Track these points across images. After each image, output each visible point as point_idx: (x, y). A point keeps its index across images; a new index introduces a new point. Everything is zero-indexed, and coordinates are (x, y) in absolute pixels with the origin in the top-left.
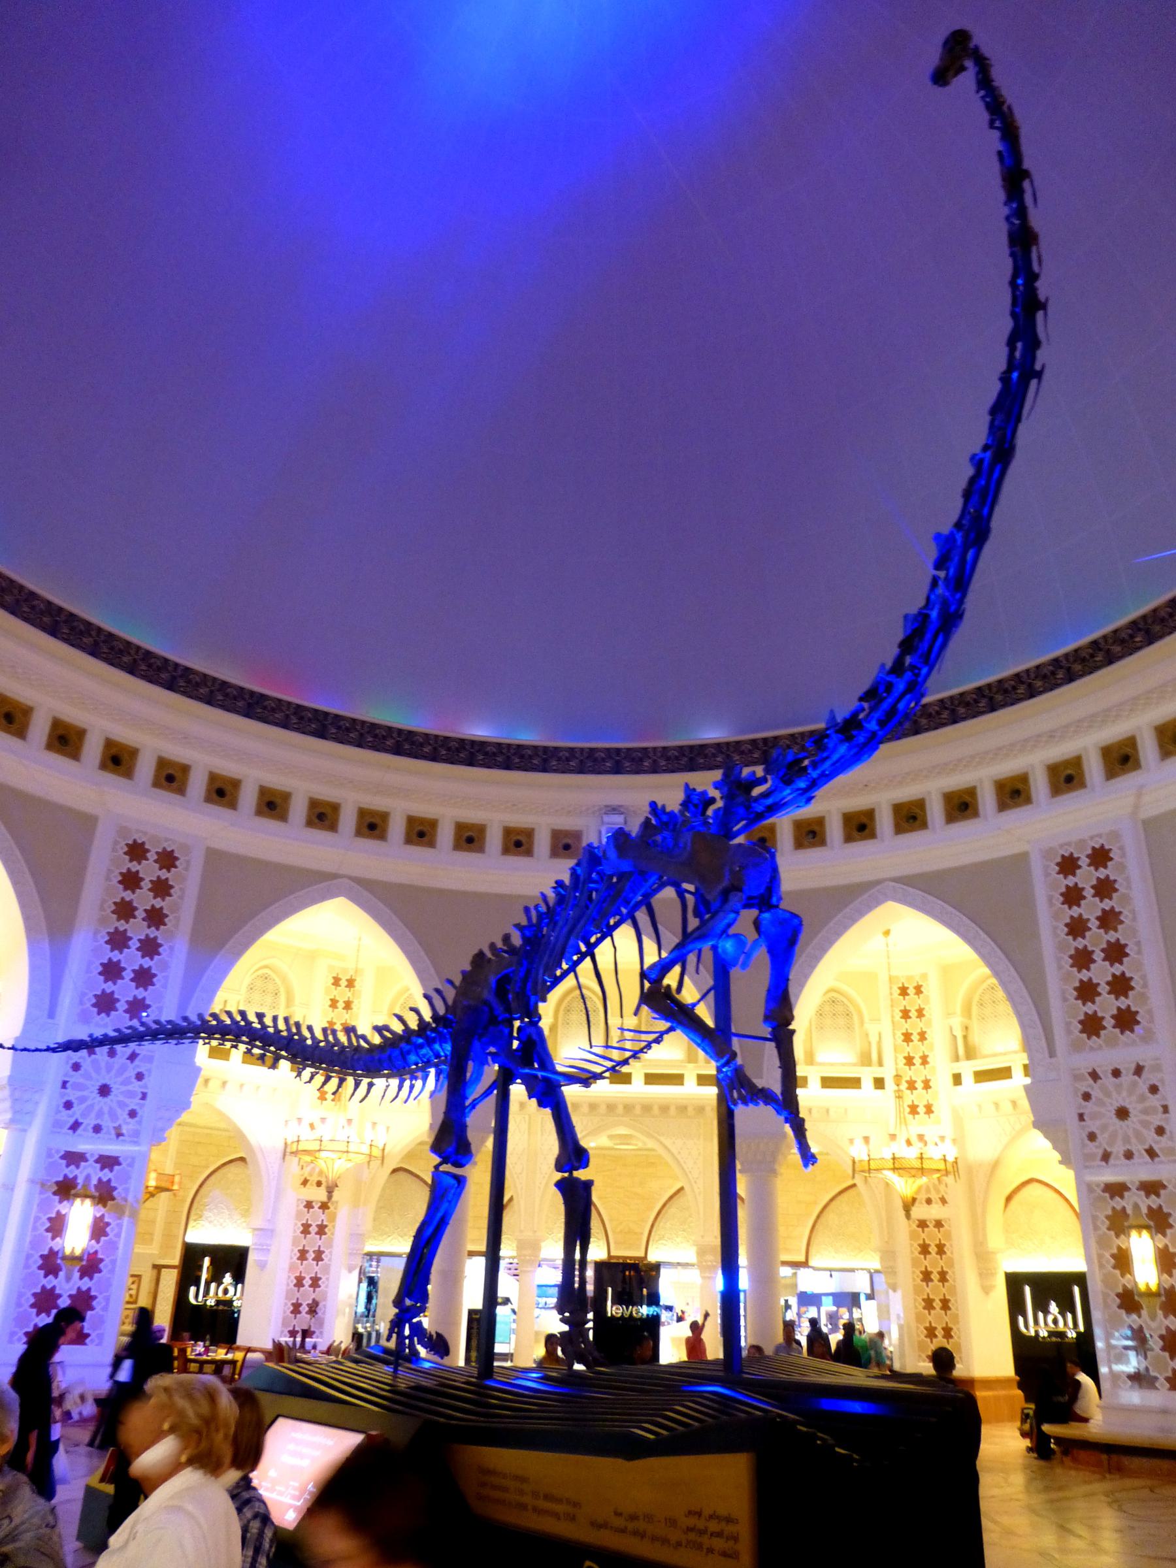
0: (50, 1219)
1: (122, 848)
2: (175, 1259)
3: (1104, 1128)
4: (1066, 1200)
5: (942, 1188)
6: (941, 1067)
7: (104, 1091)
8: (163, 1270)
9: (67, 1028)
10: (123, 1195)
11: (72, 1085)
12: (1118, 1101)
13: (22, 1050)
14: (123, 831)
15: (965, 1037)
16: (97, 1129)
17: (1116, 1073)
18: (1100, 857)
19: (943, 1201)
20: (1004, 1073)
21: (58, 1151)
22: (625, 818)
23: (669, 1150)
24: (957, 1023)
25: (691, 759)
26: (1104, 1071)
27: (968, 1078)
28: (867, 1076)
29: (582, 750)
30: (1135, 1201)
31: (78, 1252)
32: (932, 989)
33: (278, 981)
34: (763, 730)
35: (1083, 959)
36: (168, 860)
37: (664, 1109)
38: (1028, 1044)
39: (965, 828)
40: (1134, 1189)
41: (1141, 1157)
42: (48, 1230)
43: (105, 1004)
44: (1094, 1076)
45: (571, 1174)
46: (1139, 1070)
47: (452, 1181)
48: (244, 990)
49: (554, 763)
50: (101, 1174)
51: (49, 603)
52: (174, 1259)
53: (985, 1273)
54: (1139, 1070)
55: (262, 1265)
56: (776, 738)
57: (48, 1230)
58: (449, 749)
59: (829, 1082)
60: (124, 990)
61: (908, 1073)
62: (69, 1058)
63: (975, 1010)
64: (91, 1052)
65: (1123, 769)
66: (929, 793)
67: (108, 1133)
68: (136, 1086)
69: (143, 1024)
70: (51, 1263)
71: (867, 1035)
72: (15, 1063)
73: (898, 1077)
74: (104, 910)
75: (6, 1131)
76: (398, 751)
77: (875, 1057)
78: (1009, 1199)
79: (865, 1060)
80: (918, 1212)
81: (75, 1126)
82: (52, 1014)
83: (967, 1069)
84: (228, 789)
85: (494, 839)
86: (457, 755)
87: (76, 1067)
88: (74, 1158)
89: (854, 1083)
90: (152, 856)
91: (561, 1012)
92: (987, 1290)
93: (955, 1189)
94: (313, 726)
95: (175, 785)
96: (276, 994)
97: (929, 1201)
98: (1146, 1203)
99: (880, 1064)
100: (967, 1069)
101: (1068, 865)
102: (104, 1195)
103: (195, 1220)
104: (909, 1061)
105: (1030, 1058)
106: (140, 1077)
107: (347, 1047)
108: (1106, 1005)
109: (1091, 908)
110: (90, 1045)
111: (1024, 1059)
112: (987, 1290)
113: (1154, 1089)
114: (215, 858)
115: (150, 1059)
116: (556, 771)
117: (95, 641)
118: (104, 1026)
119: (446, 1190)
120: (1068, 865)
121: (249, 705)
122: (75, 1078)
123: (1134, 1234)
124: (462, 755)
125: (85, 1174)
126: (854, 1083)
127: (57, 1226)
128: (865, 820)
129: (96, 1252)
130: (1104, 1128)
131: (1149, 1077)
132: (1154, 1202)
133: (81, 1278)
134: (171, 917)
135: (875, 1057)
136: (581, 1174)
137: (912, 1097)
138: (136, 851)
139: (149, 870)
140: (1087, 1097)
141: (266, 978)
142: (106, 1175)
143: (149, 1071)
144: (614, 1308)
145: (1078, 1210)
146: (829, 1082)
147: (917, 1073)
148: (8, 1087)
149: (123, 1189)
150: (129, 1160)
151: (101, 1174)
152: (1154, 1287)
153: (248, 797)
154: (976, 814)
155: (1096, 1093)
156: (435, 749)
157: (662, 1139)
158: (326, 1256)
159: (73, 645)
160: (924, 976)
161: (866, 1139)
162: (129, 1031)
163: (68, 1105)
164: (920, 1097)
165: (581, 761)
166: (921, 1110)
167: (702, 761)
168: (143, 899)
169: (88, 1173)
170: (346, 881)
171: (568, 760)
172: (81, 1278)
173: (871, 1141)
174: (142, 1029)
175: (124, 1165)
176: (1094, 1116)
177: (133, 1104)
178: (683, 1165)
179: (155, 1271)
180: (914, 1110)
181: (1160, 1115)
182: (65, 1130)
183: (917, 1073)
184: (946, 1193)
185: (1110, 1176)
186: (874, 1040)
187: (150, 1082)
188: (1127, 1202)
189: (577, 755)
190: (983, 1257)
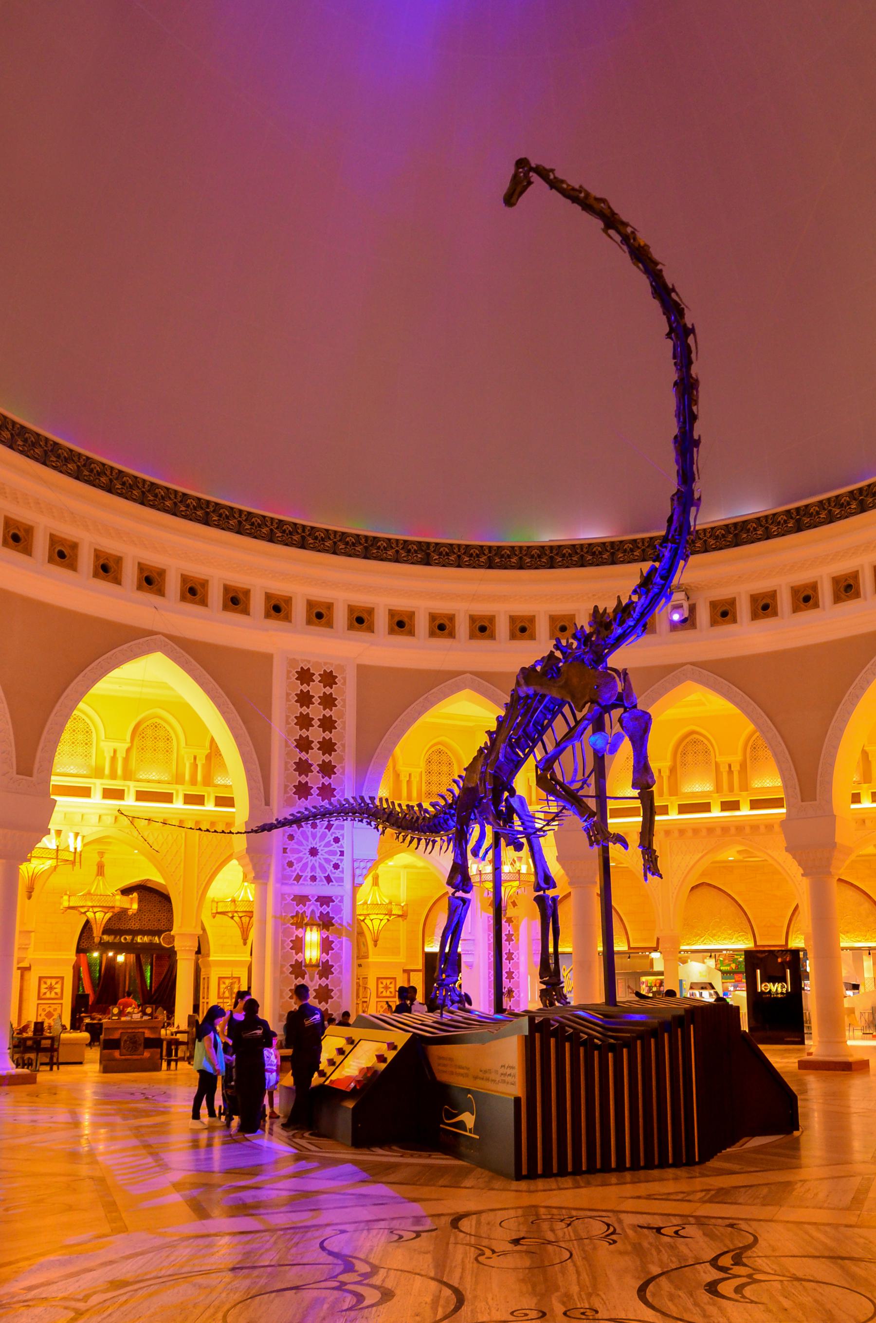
1: (294, 676)
2: (420, 964)
7: (314, 852)
8: (411, 973)
9: (278, 811)
10: (339, 922)
11: (290, 850)
13: (236, 833)
14: (292, 662)
16: (313, 879)
22: (686, 594)
23: (776, 860)
25: (736, 535)
29: (643, 540)
31: (314, 961)
33: (449, 753)
34: (796, 501)
36: (329, 679)
37: (696, 831)
39: (808, 616)
40: (313, 900)
43: (303, 790)
45: (544, 892)
47: (460, 902)
48: (422, 764)
49: (621, 555)
50: (321, 909)
51: (199, 499)
52: (418, 965)
55: (470, 966)
56: (807, 506)
58: (532, 557)
60: (315, 780)
62: (285, 832)
64: (300, 826)
65: (724, 621)
66: (821, 577)
67: (321, 881)
68: (335, 847)
69: (331, 804)
70: (299, 969)
72: (247, 838)
74: (289, 724)
75: (253, 886)
76: (490, 565)
82: (267, 803)
84: (365, 616)
86: (540, 561)
87: (291, 837)
88: (302, 899)
90: (317, 678)
91: (679, 755)
94: (419, 556)
95: (324, 620)
96: (450, 764)
98: (319, 909)
102: (326, 922)
103: (430, 936)
106: (337, 840)
110: (296, 821)
114: (363, 671)
115: (342, 827)
116: (622, 562)
117: (239, 521)
118: (301, 806)
119: (457, 907)
121: (366, 548)
122: (293, 845)
124: (544, 560)
125: (310, 910)
127: (299, 945)
128: (809, 592)
129: (327, 961)
133: (320, 979)
134: (339, 722)
136: (551, 893)
138: (305, 676)
139: (317, 689)
141: (440, 752)
142: (325, 909)
143: (343, 835)
144: (763, 985)
148: (247, 855)
150: (340, 898)
151: (321, 909)
153: (381, 621)
154: (816, 605)
156: (521, 558)
157: (769, 852)
158: (515, 956)
159: (223, 529)
162: (299, 815)
163: (291, 864)
165: (643, 551)
167: (745, 536)
168: (316, 711)
171: (632, 550)
172: (320, 979)
174: (306, 813)
175: (336, 901)
177: (335, 859)
178: (789, 872)
179: (406, 975)
181: (338, 857)
184: (517, 899)
187: (345, 843)
189: (639, 545)
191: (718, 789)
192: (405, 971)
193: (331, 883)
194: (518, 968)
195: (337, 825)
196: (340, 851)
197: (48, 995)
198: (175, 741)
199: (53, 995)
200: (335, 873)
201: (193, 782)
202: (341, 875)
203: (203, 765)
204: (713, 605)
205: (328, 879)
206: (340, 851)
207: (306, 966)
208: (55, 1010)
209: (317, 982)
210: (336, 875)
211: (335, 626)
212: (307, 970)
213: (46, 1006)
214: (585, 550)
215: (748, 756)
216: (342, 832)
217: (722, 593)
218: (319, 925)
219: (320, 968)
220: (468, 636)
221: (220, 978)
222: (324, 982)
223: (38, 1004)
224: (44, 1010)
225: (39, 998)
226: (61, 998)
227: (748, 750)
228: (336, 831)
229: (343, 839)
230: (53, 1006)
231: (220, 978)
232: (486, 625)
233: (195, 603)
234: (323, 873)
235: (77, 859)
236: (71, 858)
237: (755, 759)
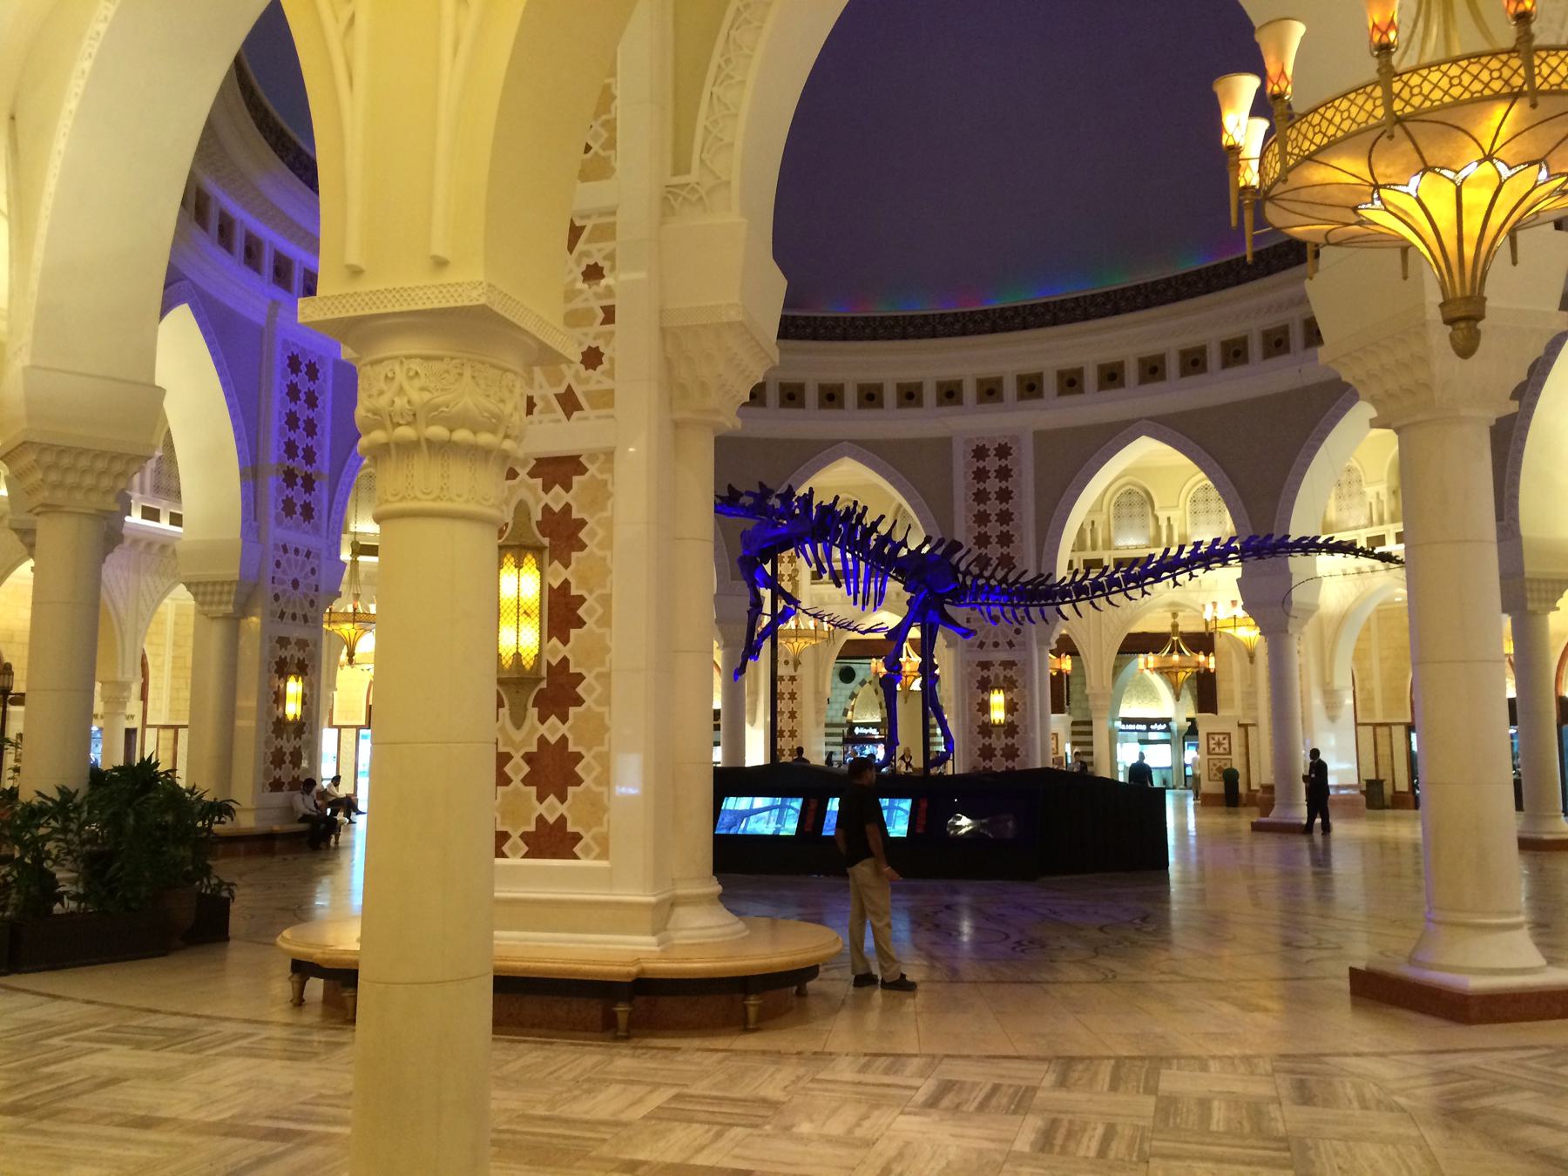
0: (978, 704)
18: (1003, 451)
21: (974, 662)
31: (996, 691)
35: (1005, 517)
42: (979, 710)
57: (979, 710)
67: (548, 409)
81: (982, 645)
85: (890, 395)
88: (985, 665)
101: (980, 453)
102: (1008, 685)
109: (992, 485)
120: (980, 453)
130: (996, 635)
139: (992, 463)
143: (611, 257)
149: (594, 757)
151: (547, 499)
161: (1214, 604)
169: (997, 671)
170: (1144, 422)
172: (542, 720)
173: (1218, 606)
182: (975, 648)
188: (991, 674)
192: (1240, 725)
193: (576, 414)
195: (596, 227)
196: (604, 308)
197: (1217, 750)
199: (1222, 751)
200: (587, 381)
202: (607, 384)
205: (1011, 644)
206: (604, 308)
208: (1215, 765)
209: (533, 727)
210: (592, 387)
213: (1216, 762)
216: (607, 246)
219: (544, 685)
221: (1208, 734)
222: (1010, 741)
223: (1209, 760)
224: (1215, 765)
225: (1209, 753)
226: (1230, 753)
228: (593, 247)
229: (613, 268)
230: (1223, 762)
231: (1208, 734)
234: (552, 386)
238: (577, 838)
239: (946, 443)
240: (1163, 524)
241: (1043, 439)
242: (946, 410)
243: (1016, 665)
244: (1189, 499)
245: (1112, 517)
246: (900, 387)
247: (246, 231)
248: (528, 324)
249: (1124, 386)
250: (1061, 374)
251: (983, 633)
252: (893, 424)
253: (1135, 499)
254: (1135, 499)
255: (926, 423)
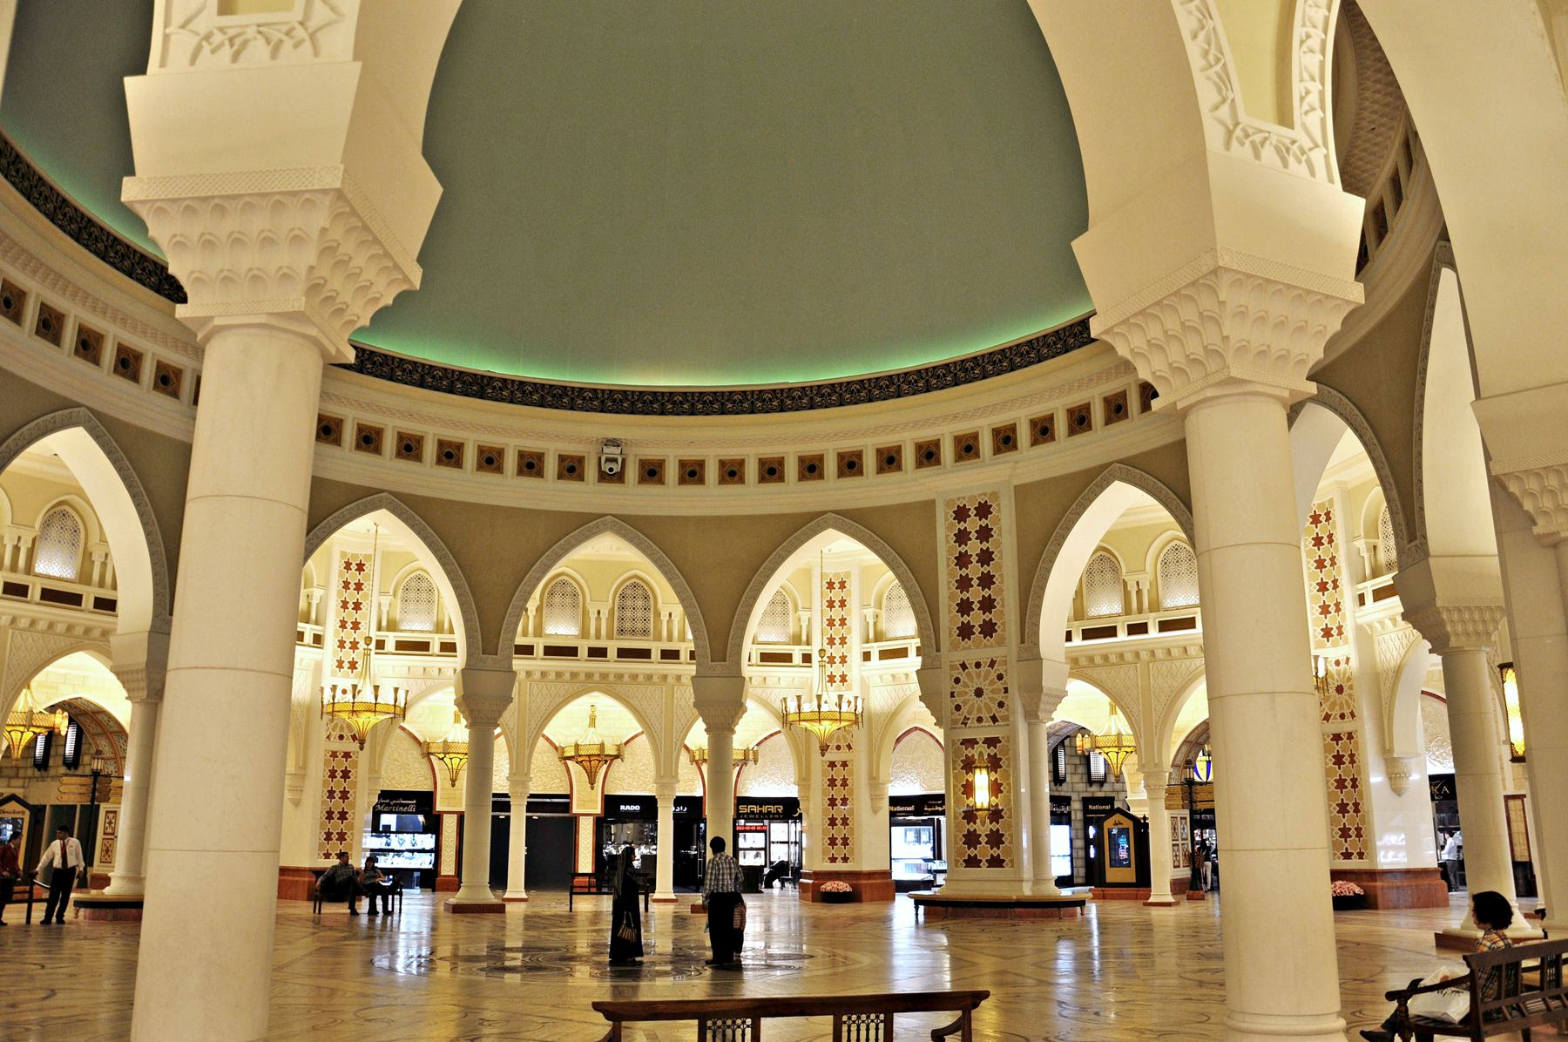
3: (966, 685)
4: (937, 741)
5: (849, 737)
6: (855, 648)
12: (978, 684)
15: (875, 623)
17: (978, 665)
18: (984, 510)
19: (849, 747)
20: (902, 653)
24: (870, 613)
26: (970, 663)
27: (875, 655)
28: (797, 652)
30: (980, 752)
32: (853, 585)
38: (921, 632)
41: (987, 722)
44: (964, 666)
46: (992, 664)
53: (875, 798)
54: (992, 664)
58: (434, 377)
59: (767, 658)
61: (829, 651)
63: (400, 591)
67: (348, 739)
68: (999, 685)
71: (799, 620)
73: (822, 651)
77: (804, 638)
78: (898, 741)
79: (796, 640)
80: (832, 755)
83: (875, 648)
88: (970, 743)
89: (787, 658)
92: (875, 811)
93: (860, 737)
97: (838, 748)
98: (987, 751)
99: (808, 643)
100: (875, 648)
101: (961, 514)
104: (831, 641)
105: (922, 642)
107: (788, 880)
108: (976, 618)
111: (917, 642)
112: (875, 811)
113: (1000, 677)
120: (961, 514)
123: (986, 805)
126: (787, 658)
127: (995, 788)
131: (999, 669)
132: (992, 751)
135: (804, 638)
137: (831, 670)
139: (973, 524)
140: (957, 681)
145: (942, 742)
146: (767, 658)
147: (836, 651)
152: (977, 771)
155: (963, 678)
160: (848, 574)
163: (958, 708)
164: (837, 670)
166: (838, 679)
172: (991, 823)
176: (960, 694)
180: (831, 679)
181: (1002, 694)
183: (836, 651)
185: (968, 734)
186: (804, 624)
188: (974, 752)
190: (875, 782)
191: (1127, 610)
194: (354, 808)
198: (581, 597)
201: (598, 637)
203: (535, 617)
204: (643, 463)
207: (978, 810)
211: (757, 461)
212: (978, 813)
214: (755, 397)
215: (545, 601)
217: (652, 453)
218: (987, 767)
220: (797, 478)
227: (1159, 566)
232: (735, 469)
233: (369, 451)
235: (860, 720)
236: (854, 718)
237: (1091, 584)
238: (1004, 861)
239: (929, 506)
240: (1133, 590)
241: (1022, 492)
242: (925, 471)
243: (1000, 742)
244: (1159, 562)
245: (616, 608)
246: (879, 452)
247: (119, 344)
248: (162, 430)
249: (901, 470)
250: (841, 456)
251: (346, 730)
252: (873, 490)
253: (1183, 555)
254: (1183, 555)
255: (910, 485)
